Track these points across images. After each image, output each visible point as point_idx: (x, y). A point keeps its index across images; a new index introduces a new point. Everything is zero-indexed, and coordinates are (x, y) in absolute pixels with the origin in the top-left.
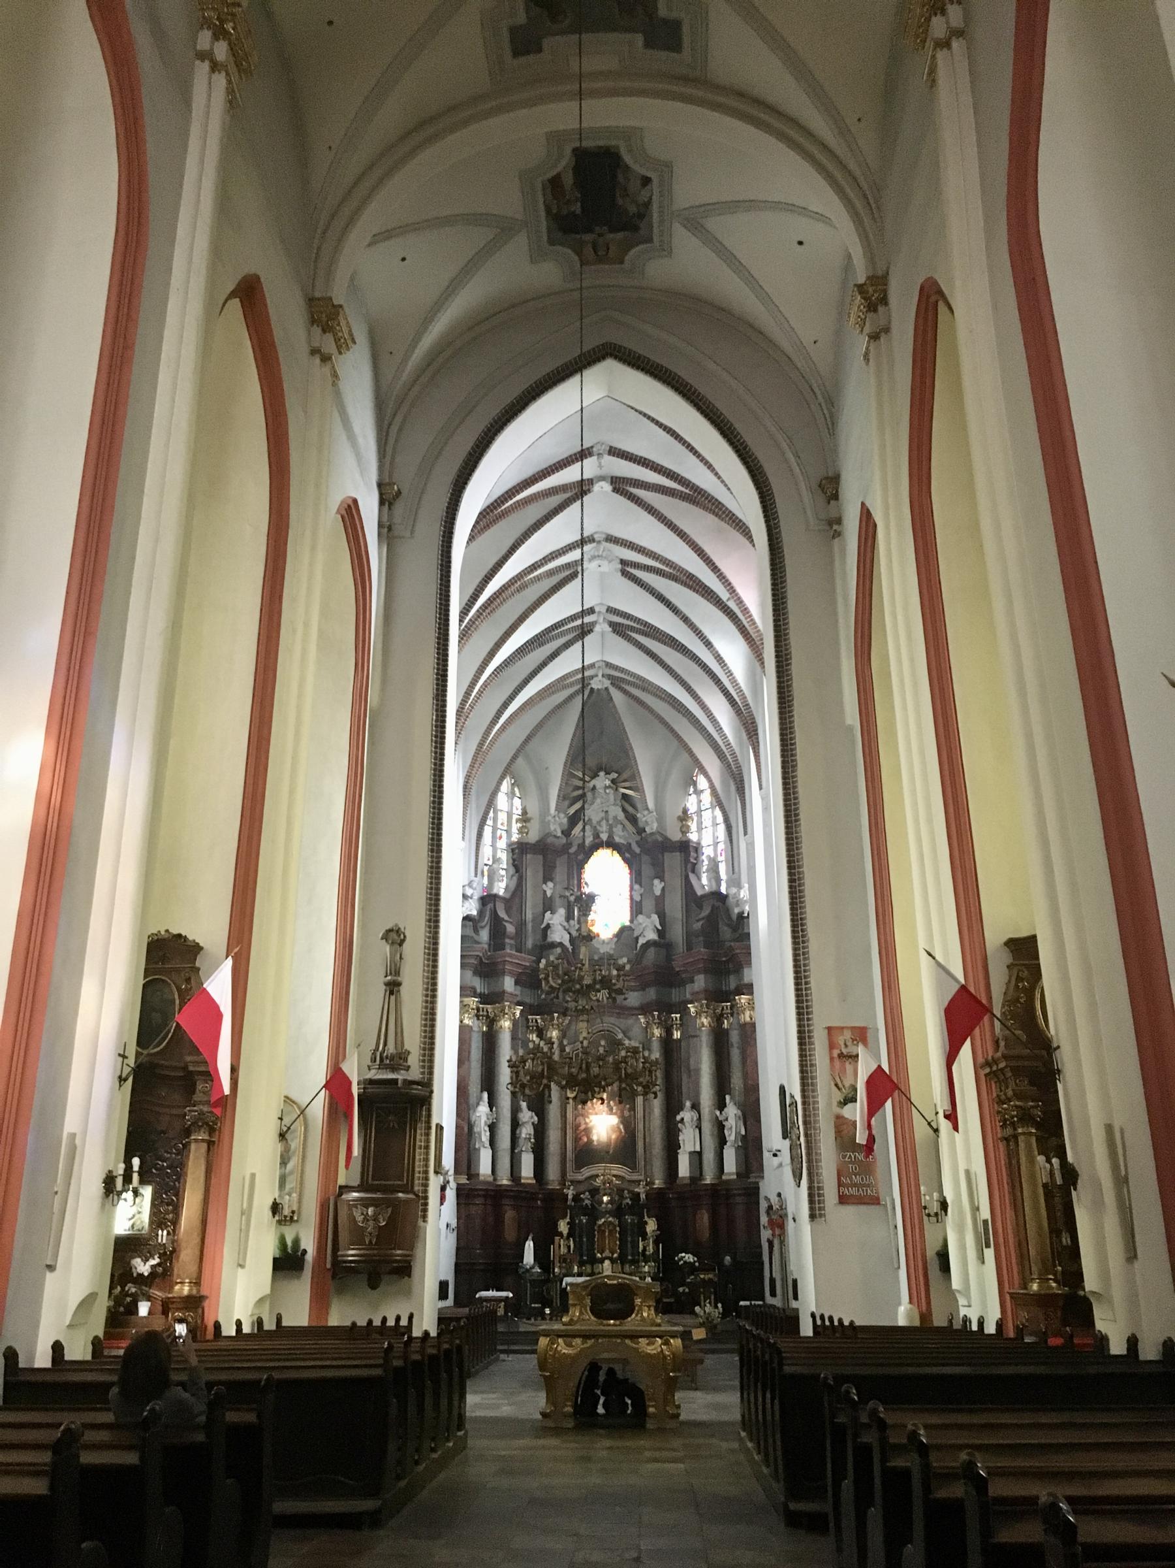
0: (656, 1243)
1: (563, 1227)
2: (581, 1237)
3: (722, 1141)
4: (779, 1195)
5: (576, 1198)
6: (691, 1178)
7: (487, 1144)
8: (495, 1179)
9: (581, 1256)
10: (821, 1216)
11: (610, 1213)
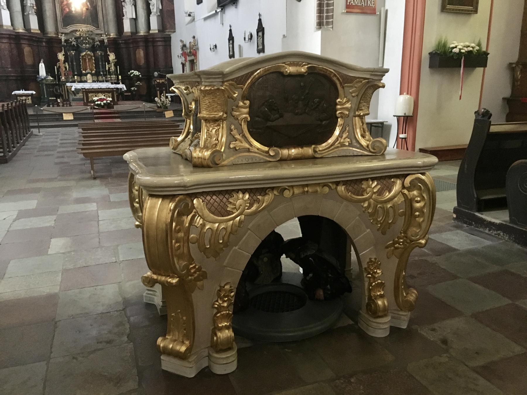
0: (115, 66)
1: (61, 56)
2: (72, 62)
3: (149, 12)
4: (194, 37)
5: (66, 41)
6: (132, 33)
7: (5, 7)
8: (14, 29)
9: (73, 72)
10: (328, 23)
11: (89, 49)
